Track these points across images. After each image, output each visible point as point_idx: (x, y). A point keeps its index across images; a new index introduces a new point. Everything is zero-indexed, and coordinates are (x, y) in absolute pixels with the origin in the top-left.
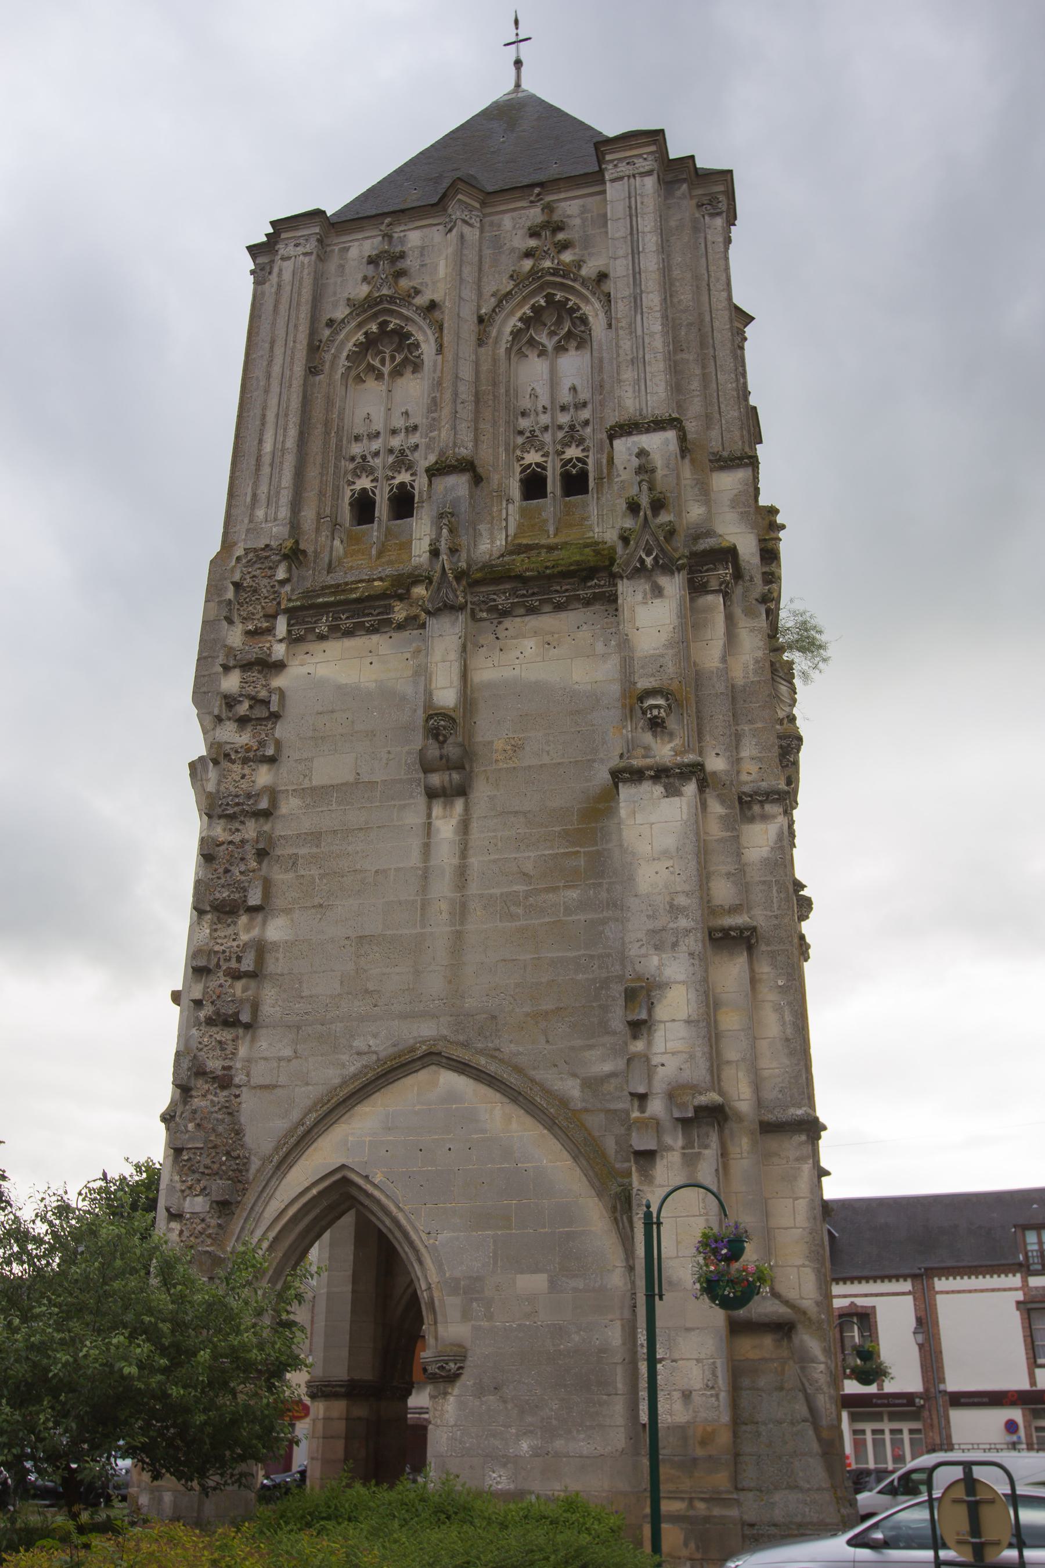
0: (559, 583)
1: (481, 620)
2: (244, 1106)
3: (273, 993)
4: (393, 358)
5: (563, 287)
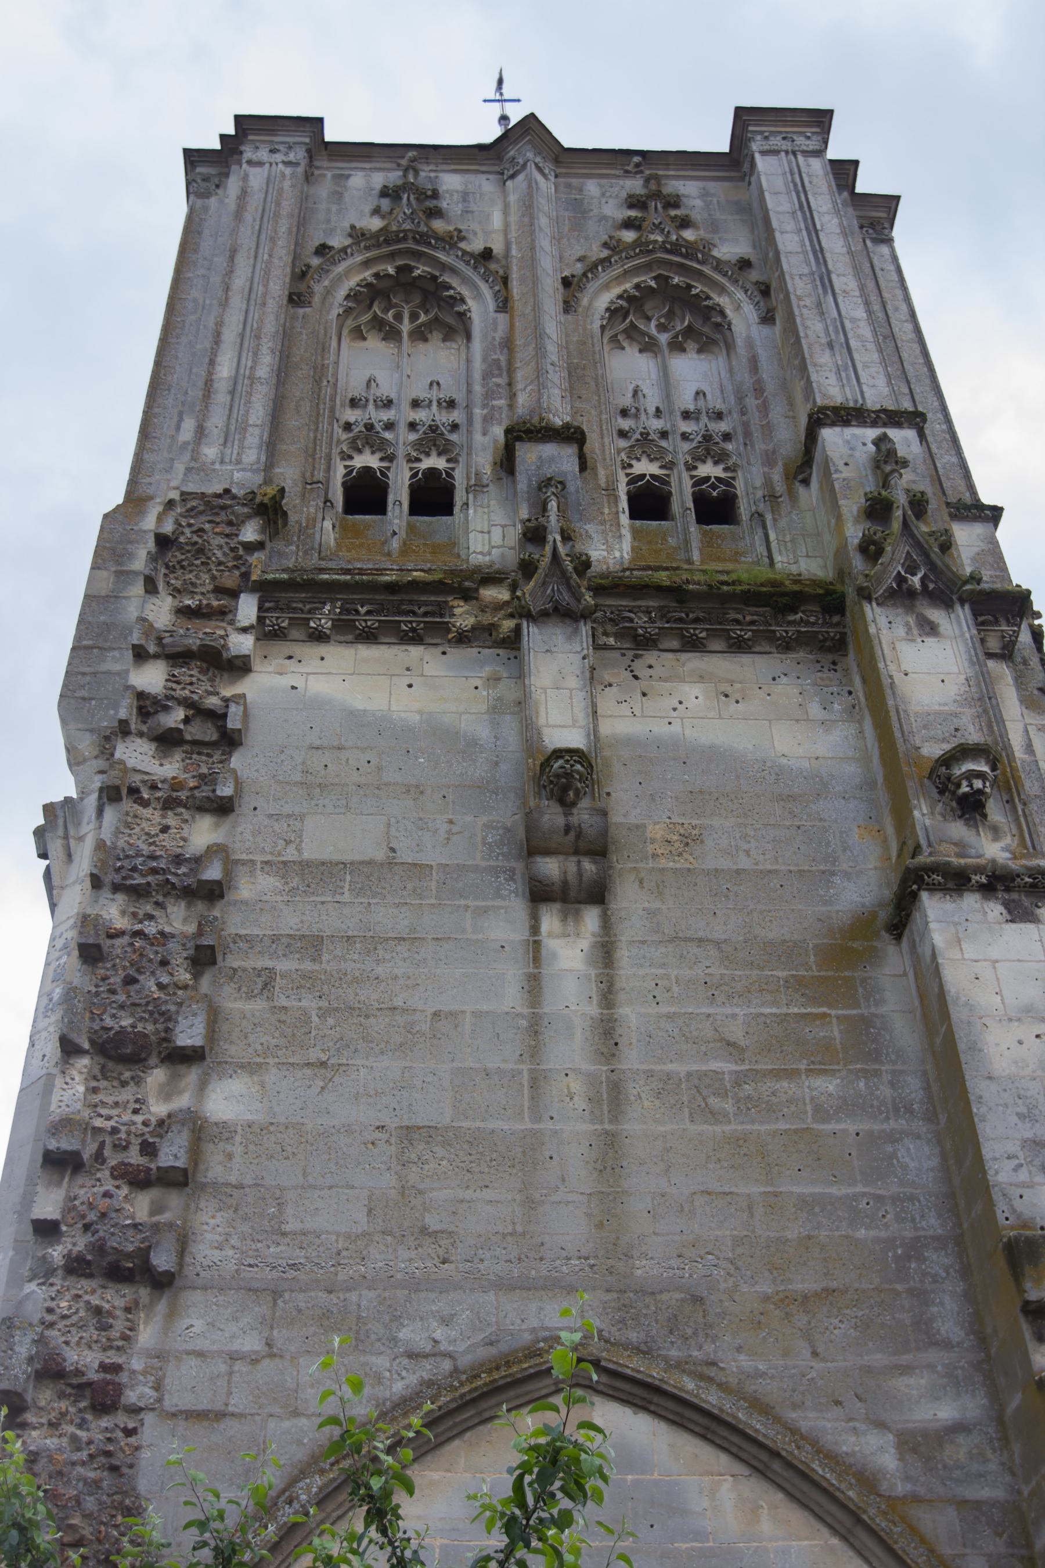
0: (739, 611)
1: (605, 647)
2: (145, 1454)
3: (218, 1220)
4: (414, 317)
5: (683, 269)
